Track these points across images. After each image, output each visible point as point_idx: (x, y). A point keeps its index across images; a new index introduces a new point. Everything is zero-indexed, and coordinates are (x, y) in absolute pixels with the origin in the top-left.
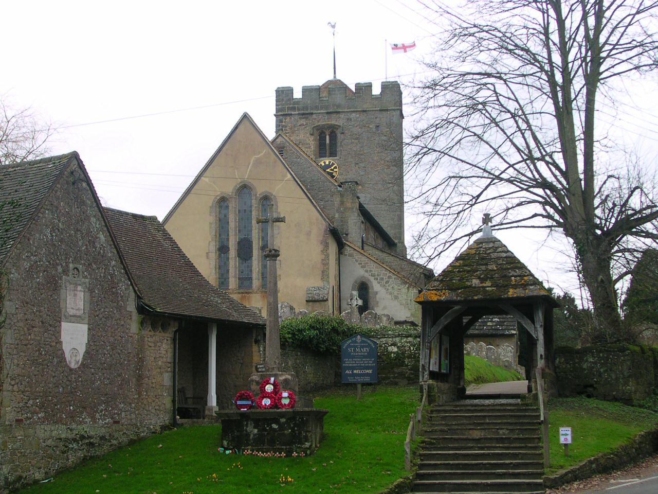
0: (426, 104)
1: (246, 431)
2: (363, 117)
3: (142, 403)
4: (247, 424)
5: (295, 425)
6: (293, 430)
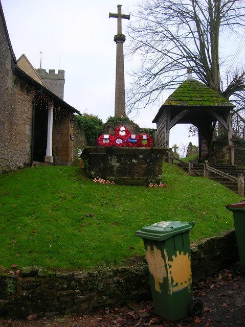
0: (147, 17)
1: (111, 164)
2: (51, 81)
3: (12, 144)
4: (111, 159)
5: (151, 161)
6: (149, 165)
